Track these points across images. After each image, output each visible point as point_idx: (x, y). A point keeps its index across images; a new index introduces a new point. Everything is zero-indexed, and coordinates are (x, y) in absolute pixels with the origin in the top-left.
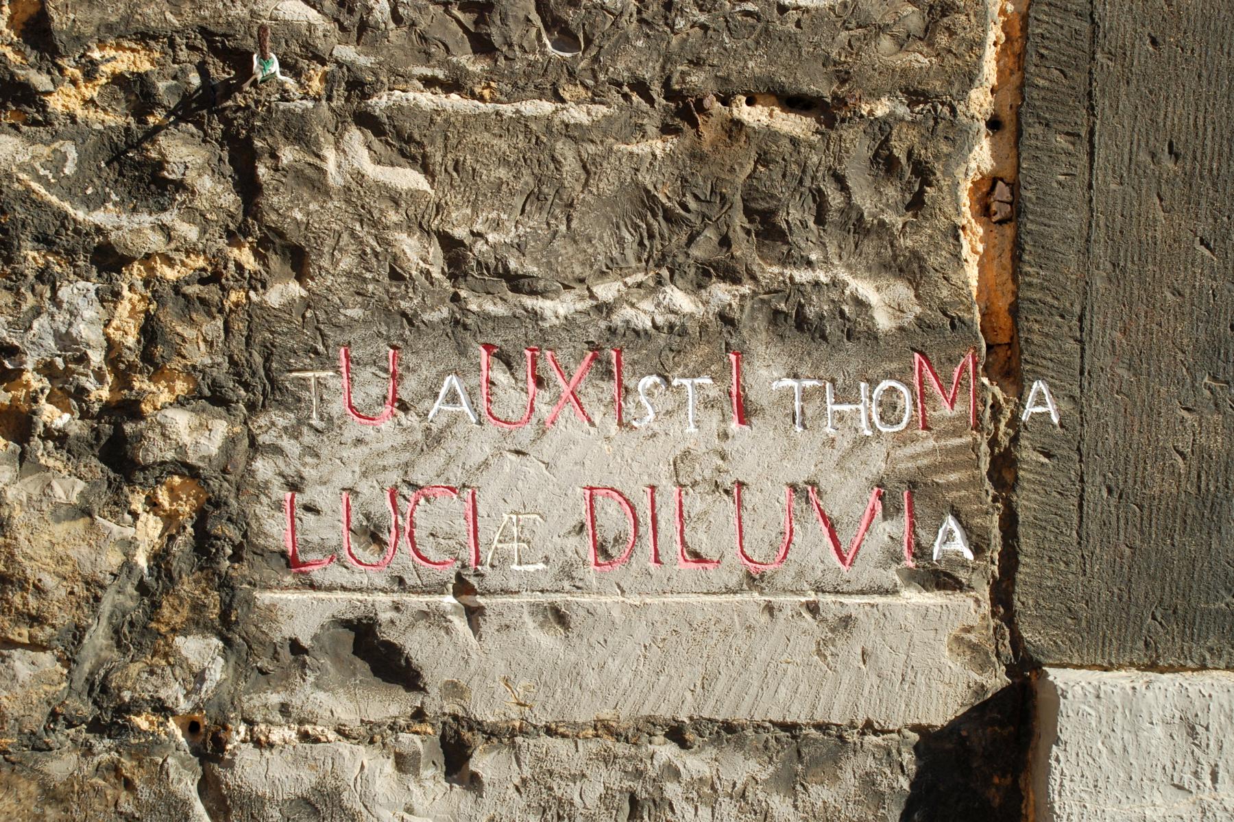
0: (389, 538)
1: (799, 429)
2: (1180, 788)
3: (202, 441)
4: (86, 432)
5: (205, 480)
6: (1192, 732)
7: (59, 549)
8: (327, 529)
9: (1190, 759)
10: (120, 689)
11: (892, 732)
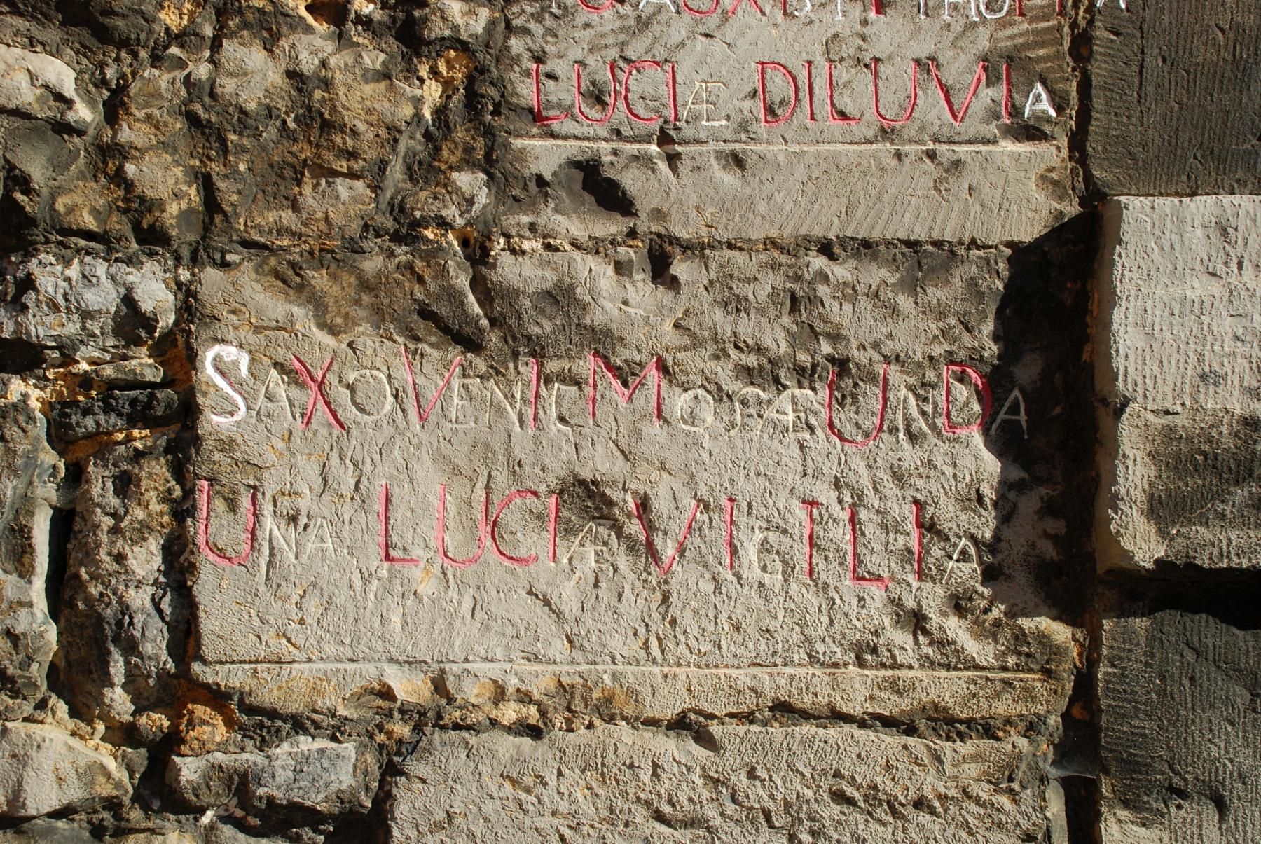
0: (610, 100)
1: (923, 17)
2: (1213, 275)
3: (471, 22)
4: (385, 18)
5: (473, 52)
6: (1224, 233)
7: (368, 103)
8: (564, 92)
9: (1222, 253)
10: (413, 209)
11: (991, 247)
